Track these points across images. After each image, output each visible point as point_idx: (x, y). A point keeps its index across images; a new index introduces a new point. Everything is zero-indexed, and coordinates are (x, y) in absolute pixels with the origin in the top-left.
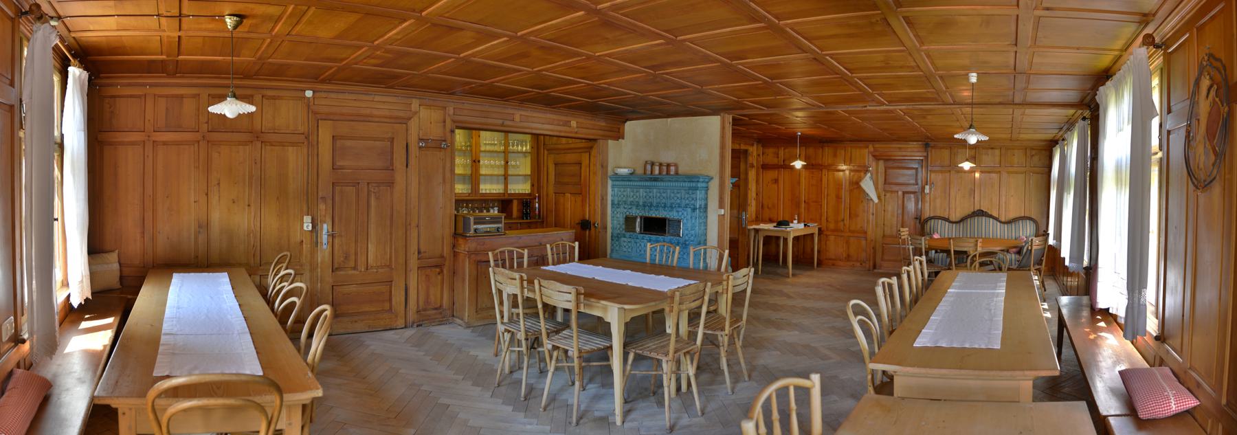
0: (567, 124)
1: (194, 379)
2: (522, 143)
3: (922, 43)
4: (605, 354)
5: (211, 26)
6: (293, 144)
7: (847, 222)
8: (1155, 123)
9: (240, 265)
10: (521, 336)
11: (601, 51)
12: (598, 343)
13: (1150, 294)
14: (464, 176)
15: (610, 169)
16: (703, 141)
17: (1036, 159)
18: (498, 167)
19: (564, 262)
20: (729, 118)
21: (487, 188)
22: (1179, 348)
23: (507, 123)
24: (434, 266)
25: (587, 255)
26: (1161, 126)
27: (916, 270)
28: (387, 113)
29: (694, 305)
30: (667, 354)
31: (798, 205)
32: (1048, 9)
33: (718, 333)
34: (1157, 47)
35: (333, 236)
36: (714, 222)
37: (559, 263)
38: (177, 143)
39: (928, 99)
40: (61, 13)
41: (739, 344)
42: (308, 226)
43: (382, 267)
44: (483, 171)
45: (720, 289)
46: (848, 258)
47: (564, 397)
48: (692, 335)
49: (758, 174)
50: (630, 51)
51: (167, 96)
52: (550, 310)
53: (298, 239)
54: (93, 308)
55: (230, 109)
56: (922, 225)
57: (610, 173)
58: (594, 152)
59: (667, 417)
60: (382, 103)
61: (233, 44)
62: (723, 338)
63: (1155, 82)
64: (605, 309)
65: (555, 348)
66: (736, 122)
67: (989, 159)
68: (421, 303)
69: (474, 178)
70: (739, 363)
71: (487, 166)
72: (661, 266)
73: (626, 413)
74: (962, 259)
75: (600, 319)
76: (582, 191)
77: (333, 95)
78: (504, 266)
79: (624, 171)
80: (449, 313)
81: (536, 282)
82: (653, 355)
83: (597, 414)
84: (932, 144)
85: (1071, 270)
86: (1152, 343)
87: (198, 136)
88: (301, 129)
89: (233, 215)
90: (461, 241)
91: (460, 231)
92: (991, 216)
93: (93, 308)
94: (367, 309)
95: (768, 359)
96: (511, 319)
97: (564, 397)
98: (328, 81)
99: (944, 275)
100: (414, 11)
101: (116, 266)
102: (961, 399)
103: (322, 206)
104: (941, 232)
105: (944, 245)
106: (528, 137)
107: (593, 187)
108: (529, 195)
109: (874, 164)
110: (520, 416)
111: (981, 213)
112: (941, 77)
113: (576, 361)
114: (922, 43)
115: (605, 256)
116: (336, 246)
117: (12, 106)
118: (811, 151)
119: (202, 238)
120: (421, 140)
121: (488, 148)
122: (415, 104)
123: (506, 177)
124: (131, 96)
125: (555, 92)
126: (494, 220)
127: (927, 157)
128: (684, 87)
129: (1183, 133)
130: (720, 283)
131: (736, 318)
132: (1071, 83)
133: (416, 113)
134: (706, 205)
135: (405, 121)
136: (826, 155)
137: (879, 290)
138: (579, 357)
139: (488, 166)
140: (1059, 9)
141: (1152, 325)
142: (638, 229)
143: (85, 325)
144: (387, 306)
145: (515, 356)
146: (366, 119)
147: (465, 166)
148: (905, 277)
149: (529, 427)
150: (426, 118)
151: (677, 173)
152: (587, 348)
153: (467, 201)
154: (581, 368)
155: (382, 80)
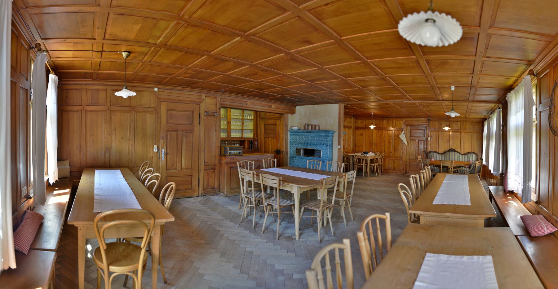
0: (270, 106)
1: (117, 211)
2: (249, 115)
3: (432, 72)
4: (290, 208)
5: (116, 56)
6: (149, 112)
7: (393, 153)
8: (534, 108)
9: (124, 167)
10: (253, 199)
11: (289, 73)
12: (287, 203)
13: (533, 184)
14: (224, 129)
15: (289, 127)
16: (330, 115)
17: (476, 126)
18: (239, 126)
19: (270, 167)
20: (342, 105)
21: (235, 135)
22: (547, 206)
23: (244, 105)
24: (211, 169)
25: (280, 165)
26: (536, 109)
27: (426, 172)
28: (191, 100)
29: (331, 186)
30: (319, 208)
31: (372, 145)
32: (488, 57)
33: (341, 200)
34: (535, 75)
35: (167, 155)
36: (335, 153)
37: (268, 168)
38: (96, 111)
39: (431, 98)
40: (48, 49)
41: (349, 205)
42: (155, 150)
43: (188, 169)
44: (232, 127)
45: (341, 180)
46: (394, 169)
47: (272, 227)
48: (329, 201)
49: (353, 131)
50: (301, 73)
51: (92, 90)
52: (266, 187)
53: (151, 156)
54: (60, 184)
55: (124, 94)
56: (427, 155)
57: (289, 129)
58: (282, 119)
59: (319, 236)
60: (189, 95)
61: (125, 65)
62: (342, 201)
63: (534, 90)
64: (291, 187)
65: (269, 205)
66: (345, 107)
67: (456, 126)
68: (205, 186)
69: (228, 130)
70: (350, 214)
71: (234, 125)
72: (313, 170)
73: (300, 234)
74: (446, 170)
75: (290, 192)
76: (276, 136)
77: (166, 91)
78: (243, 168)
79: (295, 128)
80: (217, 190)
81: (260, 175)
82: (313, 208)
83: (287, 235)
84: (431, 119)
85: (494, 175)
86: (534, 205)
87: (106, 108)
88: (153, 105)
89: (122, 145)
90: (223, 158)
91: (223, 153)
92: (457, 152)
93: (60, 184)
94: (181, 188)
95: (360, 211)
96: (247, 192)
97: (272, 227)
98: (165, 84)
99: (439, 176)
100: (207, 51)
101: (68, 167)
102: (456, 225)
103: (162, 141)
104: (435, 158)
105: (438, 163)
106: (252, 113)
107: (281, 135)
108: (253, 138)
109: (405, 128)
110: (252, 235)
111: (452, 150)
112: (439, 88)
113: (278, 210)
114: (432, 72)
115: (287, 165)
116: (168, 160)
117: (27, 90)
118: (378, 121)
119: (107, 155)
120: (206, 112)
121: (235, 117)
122: (203, 96)
123: (242, 130)
124: (76, 89)
125: (266, 92)
126: (238, 149)
127: (429, 125)
128: (324, 90)
129: (548, 112)
130: (342, 177)
131: (348, 194)
132: (494, 92)
133: (203, 100)
134: (332, 145)
135: (198, 103)
136: (384, 123)
137: (411, 180)
138: (280, 209)
139: (235, 125)
140: (493, 58)
141: (534, 197)
142: (302, 154)
143: (56, 192)
144: (190, 186)
145: (249, 209)
146: (182, 102)
147: (224, 125)
148: (422, 174)
149: (257, 240)
150: (208, 102)
151: (319, 129)
152: (283, 205)
153: (225, 141)
154: (280, 214)
155: (190, 84)
